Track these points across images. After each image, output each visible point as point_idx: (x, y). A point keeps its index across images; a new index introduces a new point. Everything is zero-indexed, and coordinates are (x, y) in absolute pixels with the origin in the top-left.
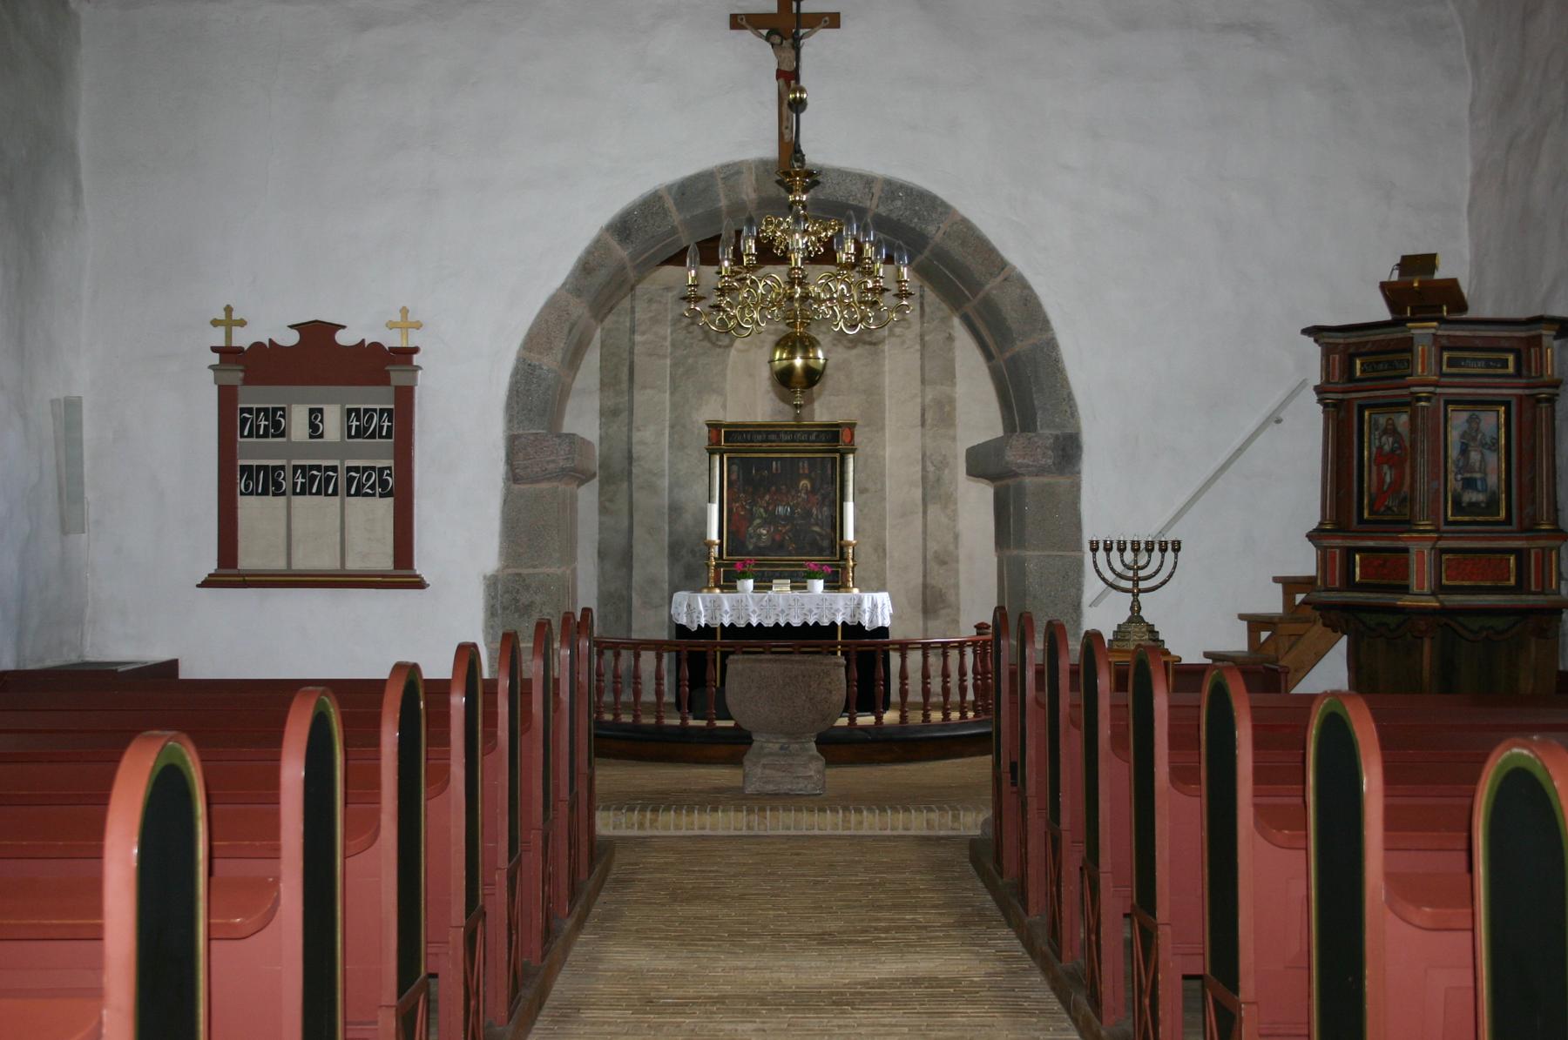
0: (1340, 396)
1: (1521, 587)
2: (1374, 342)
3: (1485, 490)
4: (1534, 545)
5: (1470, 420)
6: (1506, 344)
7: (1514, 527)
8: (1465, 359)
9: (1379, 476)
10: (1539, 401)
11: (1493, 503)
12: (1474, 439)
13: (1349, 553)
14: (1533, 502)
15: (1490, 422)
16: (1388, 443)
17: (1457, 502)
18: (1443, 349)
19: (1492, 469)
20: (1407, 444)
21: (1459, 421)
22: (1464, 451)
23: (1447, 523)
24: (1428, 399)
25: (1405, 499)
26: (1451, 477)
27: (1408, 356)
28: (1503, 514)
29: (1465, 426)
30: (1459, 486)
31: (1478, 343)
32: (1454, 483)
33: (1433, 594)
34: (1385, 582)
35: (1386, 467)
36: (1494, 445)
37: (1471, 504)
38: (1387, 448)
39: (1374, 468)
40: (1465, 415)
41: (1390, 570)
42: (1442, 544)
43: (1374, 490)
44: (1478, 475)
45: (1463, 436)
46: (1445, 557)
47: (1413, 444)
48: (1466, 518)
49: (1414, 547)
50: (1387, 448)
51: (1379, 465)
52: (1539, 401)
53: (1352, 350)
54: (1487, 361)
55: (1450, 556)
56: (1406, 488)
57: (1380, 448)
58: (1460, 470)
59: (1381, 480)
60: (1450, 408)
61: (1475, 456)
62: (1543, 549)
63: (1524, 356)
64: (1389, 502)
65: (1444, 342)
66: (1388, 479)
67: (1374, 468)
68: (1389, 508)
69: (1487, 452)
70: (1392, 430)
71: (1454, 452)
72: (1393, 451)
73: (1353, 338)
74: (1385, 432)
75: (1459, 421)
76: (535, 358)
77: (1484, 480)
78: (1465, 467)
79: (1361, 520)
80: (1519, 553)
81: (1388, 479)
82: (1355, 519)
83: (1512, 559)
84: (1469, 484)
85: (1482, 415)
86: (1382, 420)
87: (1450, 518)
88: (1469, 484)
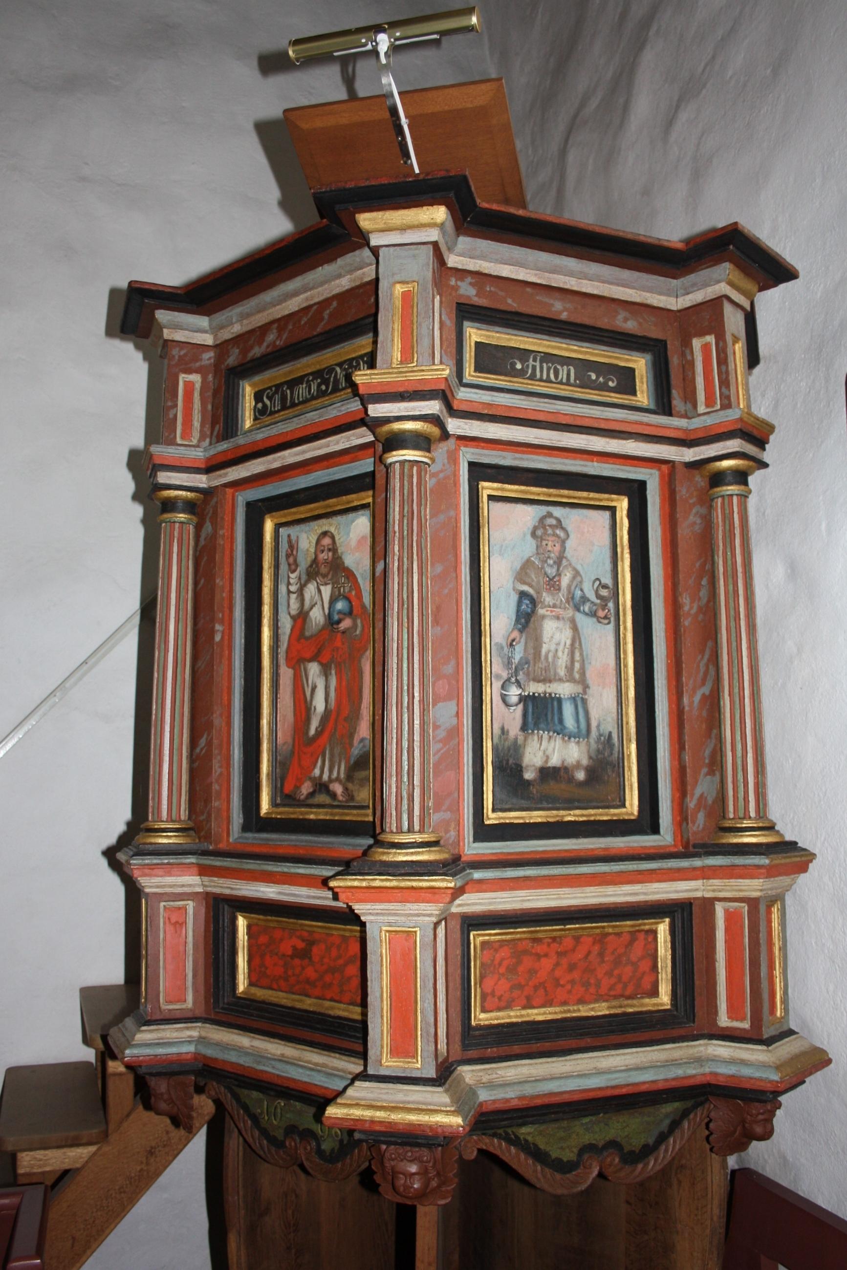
0: (201, 481)
1: (687, 1018)
2: (282, 322)
3: (583, 733)
4: (721, 890)
5: (539, 532)
6: (630, 325)
7: (666, 836)
8: (524, 354)
9: (296, 696)
10: (718, 479)
11: (603, 770)
12: (553, 584)
13: (220, 911)
14: (716, 764)
15: (591, 538)
16: (319, 600)
17: (509, 770)
18: (467, 312)
19: (594, 666)
20: (367, 599)
21: (511, 527)
22: (526, 617)
23: (484, 832)
24: (422, 442)
25: (361, 763)
26: (491, 691)
27: (363, 344)
28: (633, 804)
29: (528, 548)
30: (513, 718)
31: (560, 309)
32: (503, 716)
33: (444, 1075)
34: (308, 1004)
35: (314, 669)
36: (603, 607)
37: (547, 773)
38: (317, 616)
39: (287, 674)
40: (528, 515)
41: (314, 990)
42: (475, 902)
43: (284, 735)
44: (564, 690)
45: (523, 573)
46: (477, 938)
47: (380, 583)
48: (537, 816)
49: (381, 919)
50: (317, 616)
51: (297, 662)
52: (718, 479)
53: (232, 359)
54: (584, 366)
55: (492, 935)
56: (364, 730)
57: (301, 618)
58: (516, 673)
59: (303, 708)
60: (487, 488)
61: (554, 633)
62: (753, 903)
63: (675, 361)
64: (321, 770)
65: (467, 291)
66: (319, 704)
67: (287, 674)
68: (322, 787)
69: (586, 624)
70: (330, 567)
71: (499, 621)
72: (331, 622)
73: (676, 1033)
74: (313, 573)
75: (511, 527)
76: (562, 771)
77: (580, 702)
78: (532, 665)
79: (253, 821)
80: (686, 916)
81: (319, 704)
82: (237, 818)
83: (663, 929)
84: (540, 712)
85: (572, 518)
86: (306, 539)
87: (492, 818)
88: (540, 712)
